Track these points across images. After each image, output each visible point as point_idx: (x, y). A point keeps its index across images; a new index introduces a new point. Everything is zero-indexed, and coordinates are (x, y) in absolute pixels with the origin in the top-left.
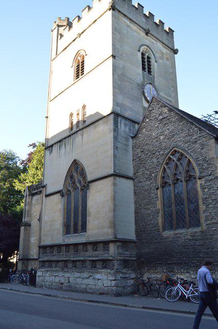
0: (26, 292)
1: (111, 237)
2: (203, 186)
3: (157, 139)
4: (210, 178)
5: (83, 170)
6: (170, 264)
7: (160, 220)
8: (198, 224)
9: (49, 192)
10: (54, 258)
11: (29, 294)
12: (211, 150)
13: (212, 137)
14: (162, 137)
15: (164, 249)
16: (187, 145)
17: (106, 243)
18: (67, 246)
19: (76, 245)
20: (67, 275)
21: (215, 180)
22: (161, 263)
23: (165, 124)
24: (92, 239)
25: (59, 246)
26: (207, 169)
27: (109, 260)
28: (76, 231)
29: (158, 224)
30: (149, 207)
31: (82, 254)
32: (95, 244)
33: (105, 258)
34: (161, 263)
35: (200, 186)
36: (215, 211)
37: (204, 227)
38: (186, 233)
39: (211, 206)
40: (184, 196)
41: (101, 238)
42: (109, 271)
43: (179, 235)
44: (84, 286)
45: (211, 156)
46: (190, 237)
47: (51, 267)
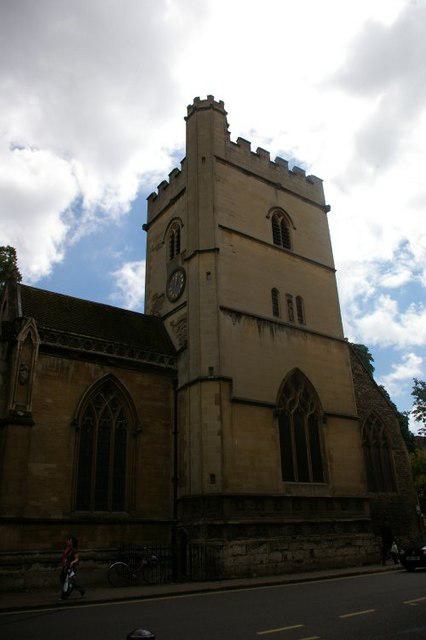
8: (394, 490)
18: (297, 500)
19: (316, 499)
20: (307, 546)
25: (278, 501)
28: (304, 478)
32: (344, 502)
44: (340, 558)
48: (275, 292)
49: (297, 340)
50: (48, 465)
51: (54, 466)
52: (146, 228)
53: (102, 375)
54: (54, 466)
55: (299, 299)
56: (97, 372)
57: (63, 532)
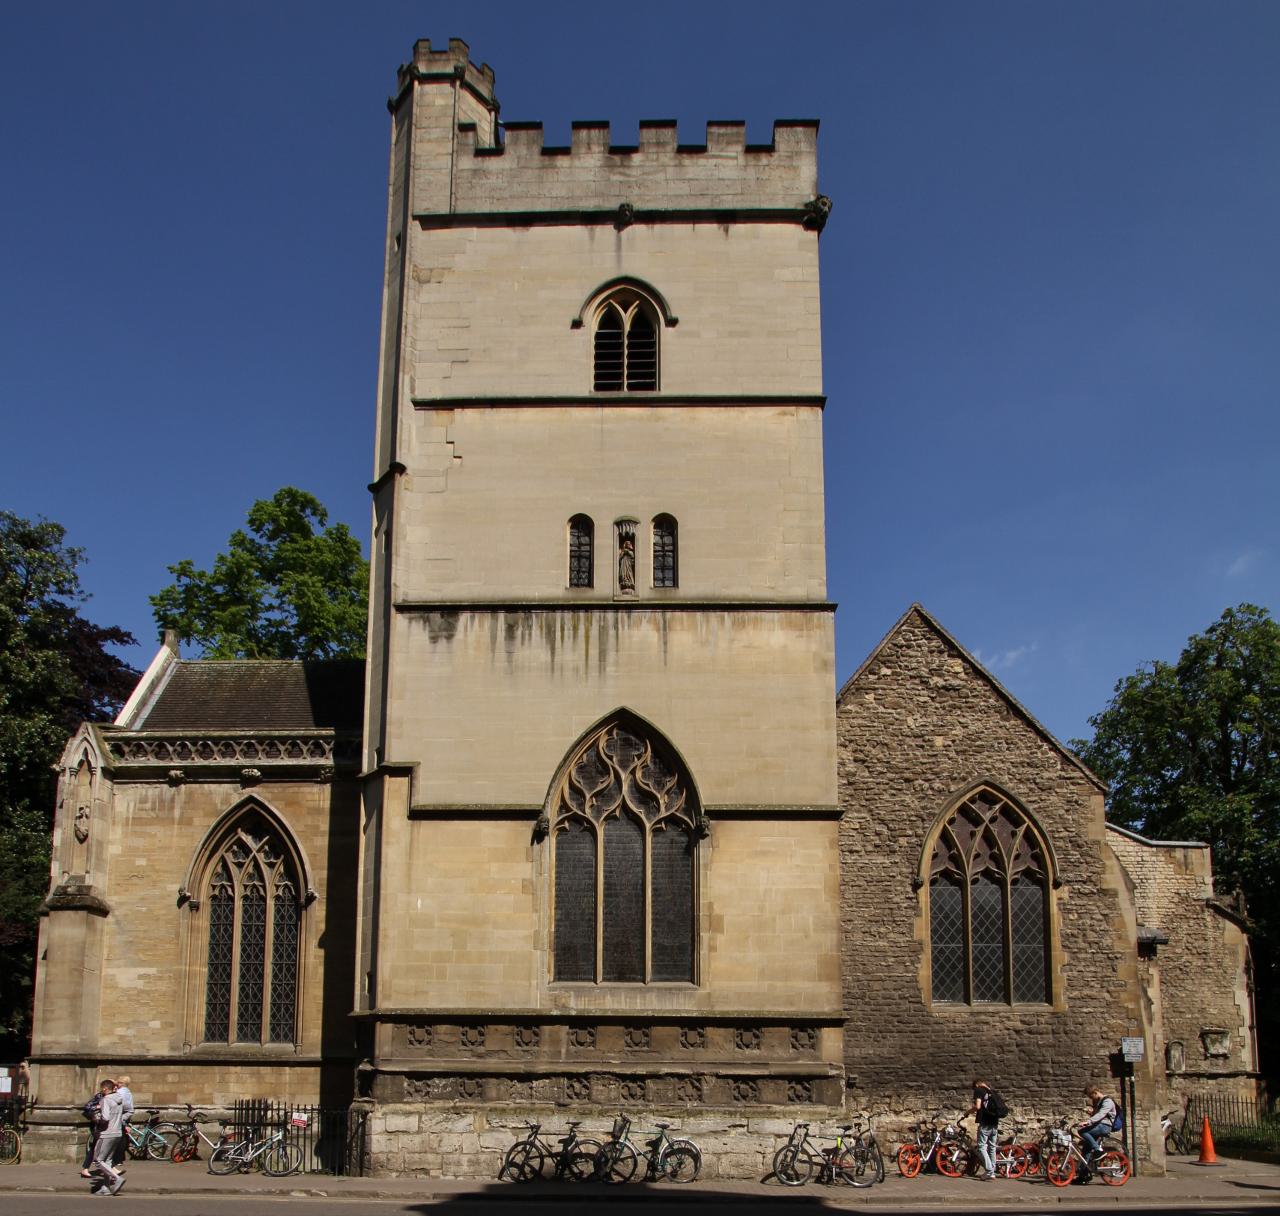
0: (206, 1191)
1: (827, 1009)
2: (1064, 904)
3: (919, 742)
4: (1088, 888)
5: (669, 761)
6: (947, 1089)
7: (924, 971)
9: (425, 798)
10: (493, 1064)
11: (141, 1196)
12: (1092, 820)
13: (1096, 790)
14: (939, 741)
15: (931, 1050)
16: (1023, 788)
17: (806, 1026)
21: (1096, 897)
22: (921, 1087)
23: (954, 707)
24: (722, 1008)
25: (528, 1023)
26: (1076, 865)
27: (827, 1077)
28: (625, 969)
29: (915, 980)
30: (882, 930)
31: (679, 1052)
32: (749, 1026)
33: (804, 1071)
34: (921, 1087)
35: (1059, 904)
36: (1093, 969)
37: (1063, 1002)
38: (1004, 1017)
39: (1083, 956)
40: (33, 859)
41: (781, 1009)
42: (822, 1108)
43: (983, 1017)
45: (1092, 837)
46: (1019, 1025)
47: (483, 1096)
48: (582, 525)
49: (686, 631)
50: (142, 971)
51: (152, 971)
52: (400, 469)
53: (236, 800)
54: (152, 971)
55: (666, 524)
56: (226, 796)
57: (170, 1078)
